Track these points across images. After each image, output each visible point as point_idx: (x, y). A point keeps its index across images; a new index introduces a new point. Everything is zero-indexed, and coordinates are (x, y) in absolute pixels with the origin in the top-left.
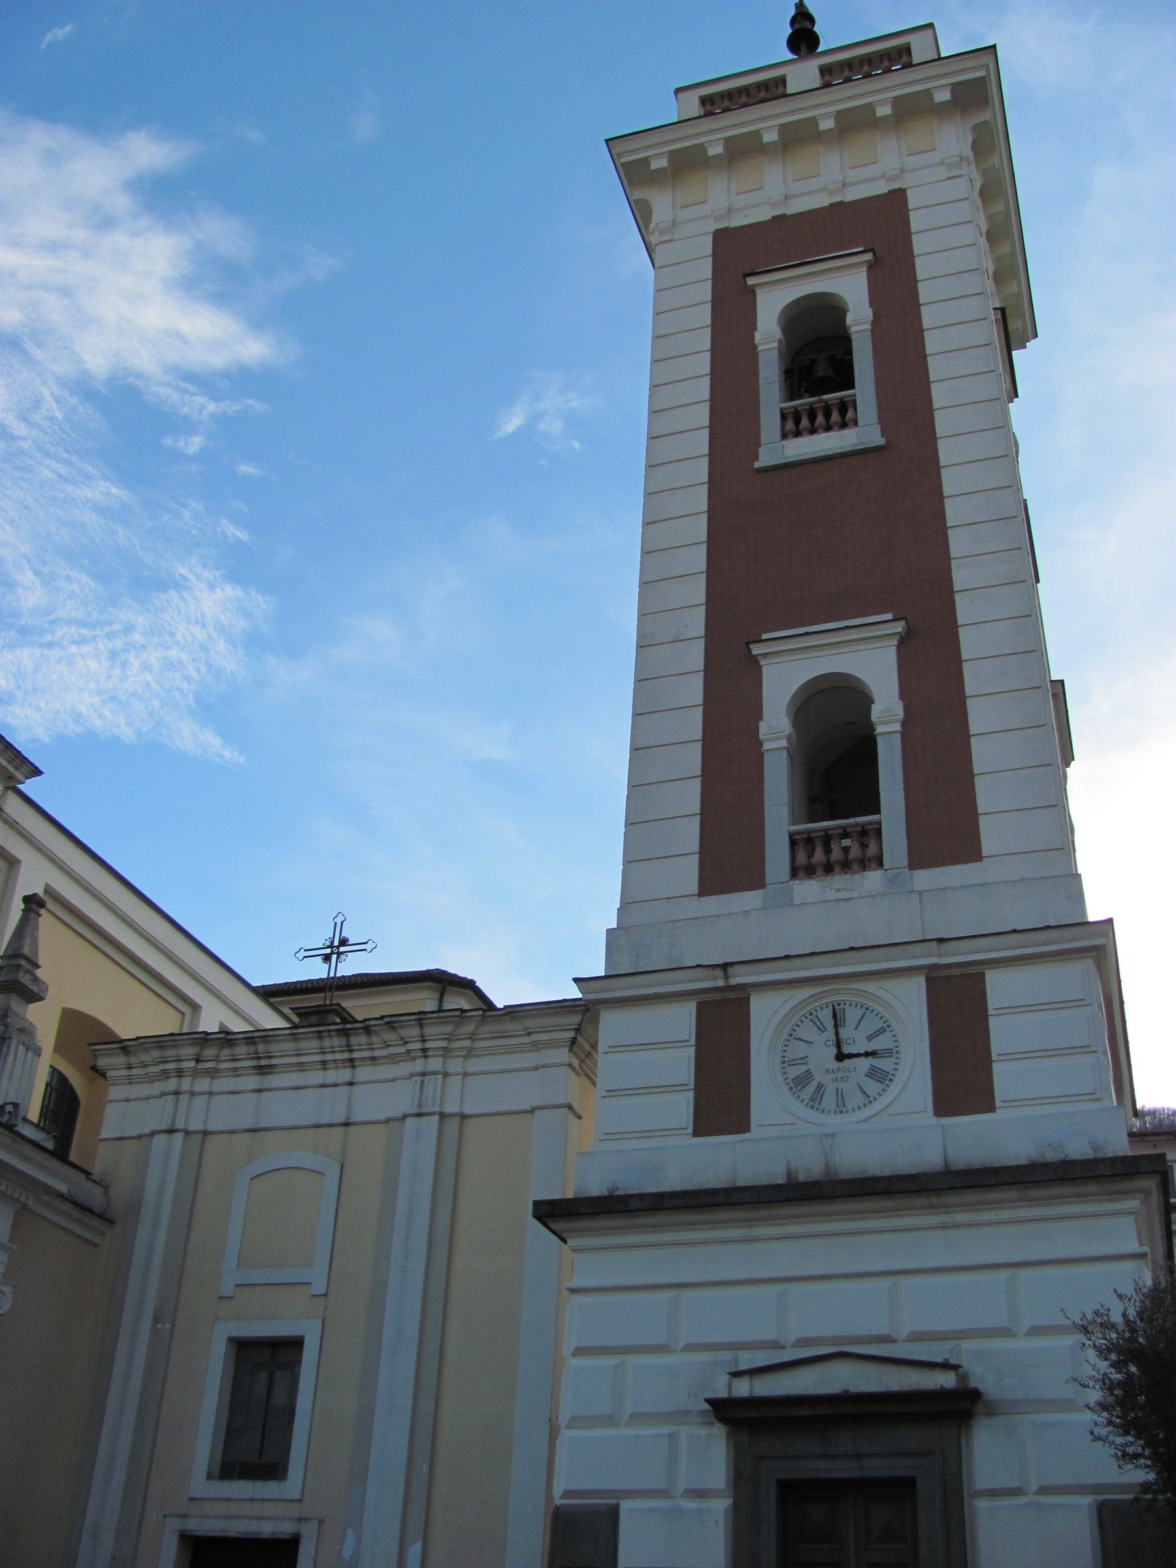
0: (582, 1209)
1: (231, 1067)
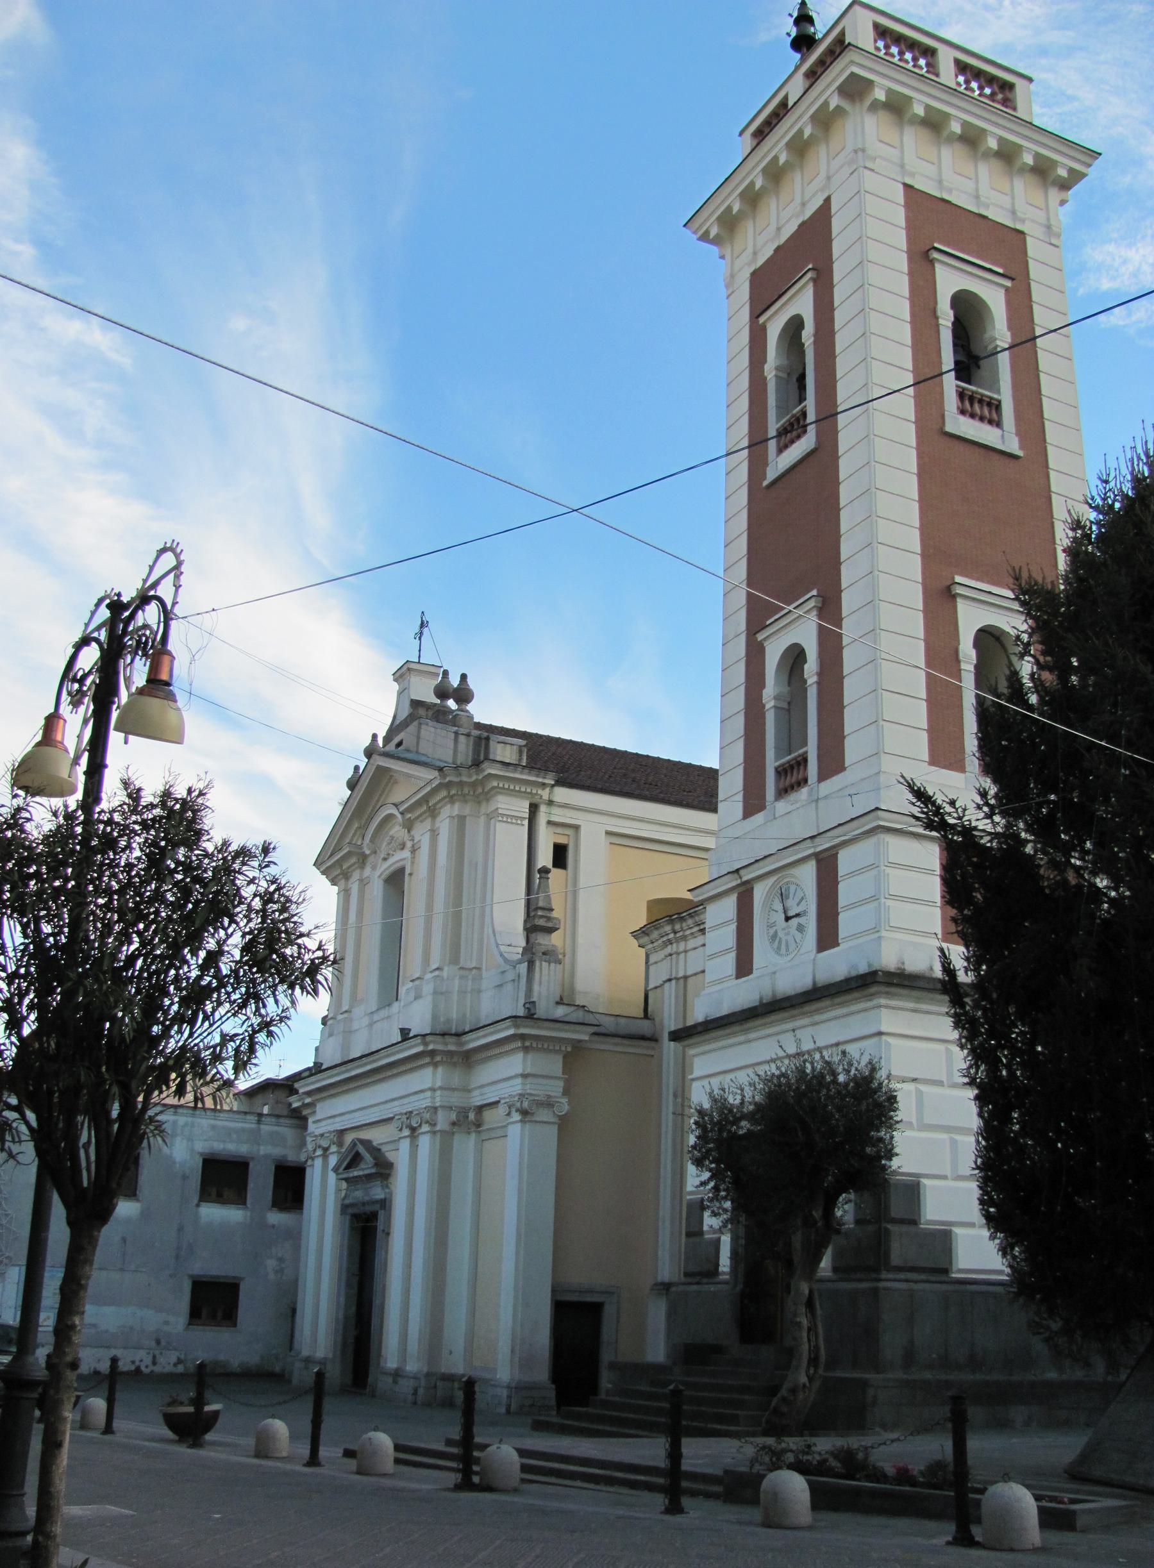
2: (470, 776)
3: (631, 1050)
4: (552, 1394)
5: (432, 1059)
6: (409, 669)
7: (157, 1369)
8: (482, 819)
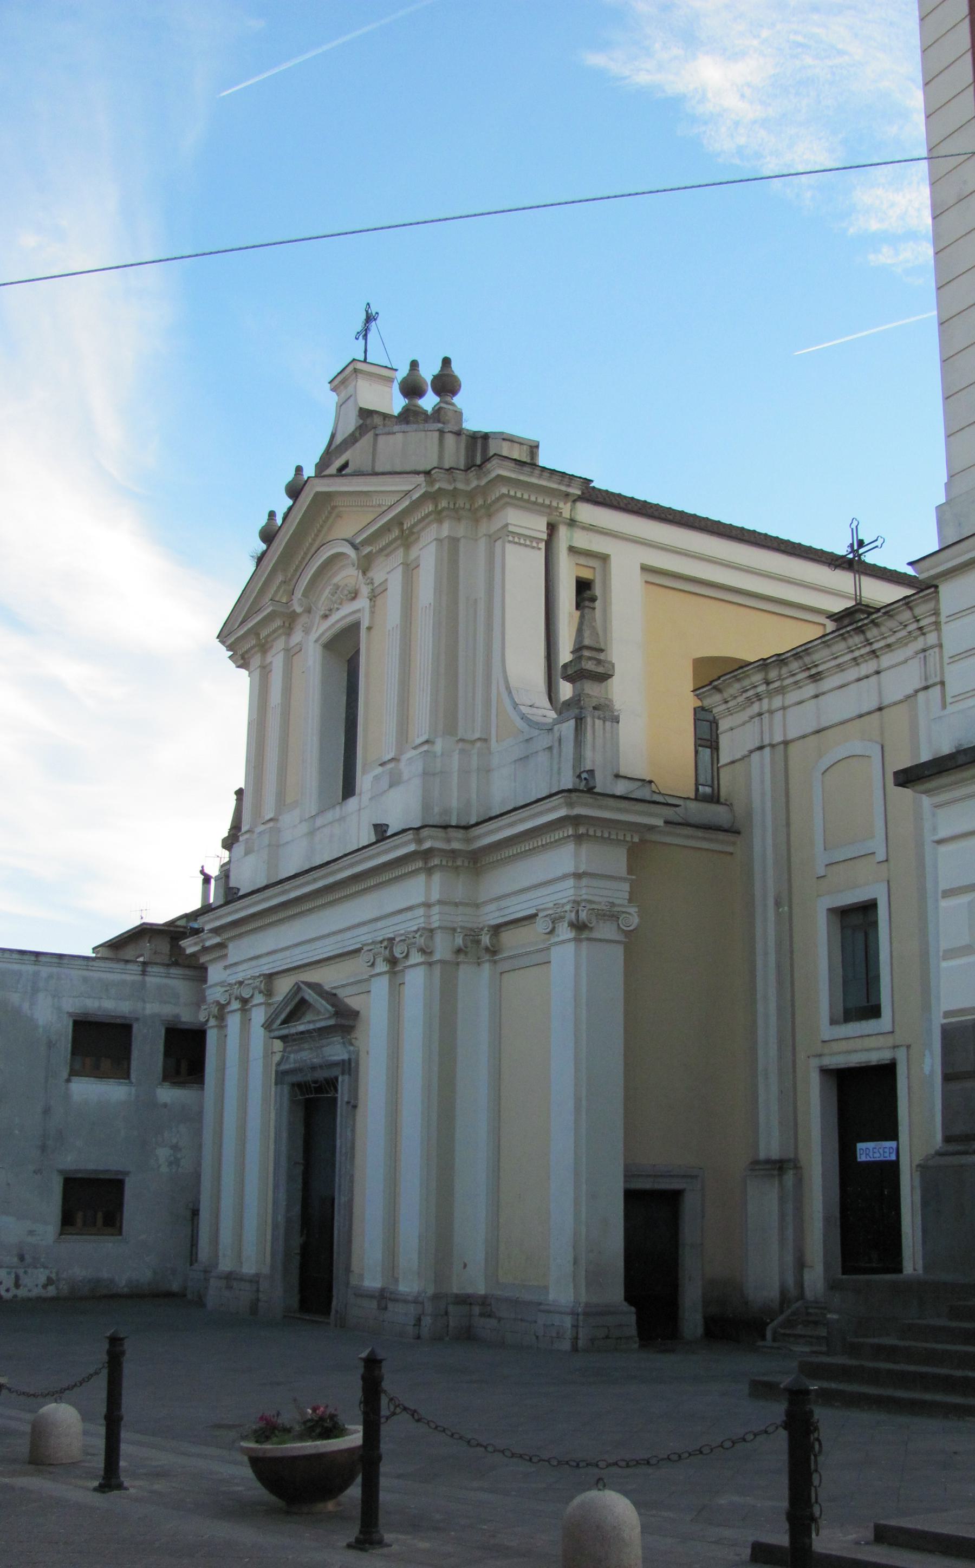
0: (926, 772)
1: (792, 681)
2: (467, 482)
3: (705, 845)
4: (629, 1317)
5: (426, 863)
6: (355, 370)
7: (22, 1293)
8: (482, 544)
